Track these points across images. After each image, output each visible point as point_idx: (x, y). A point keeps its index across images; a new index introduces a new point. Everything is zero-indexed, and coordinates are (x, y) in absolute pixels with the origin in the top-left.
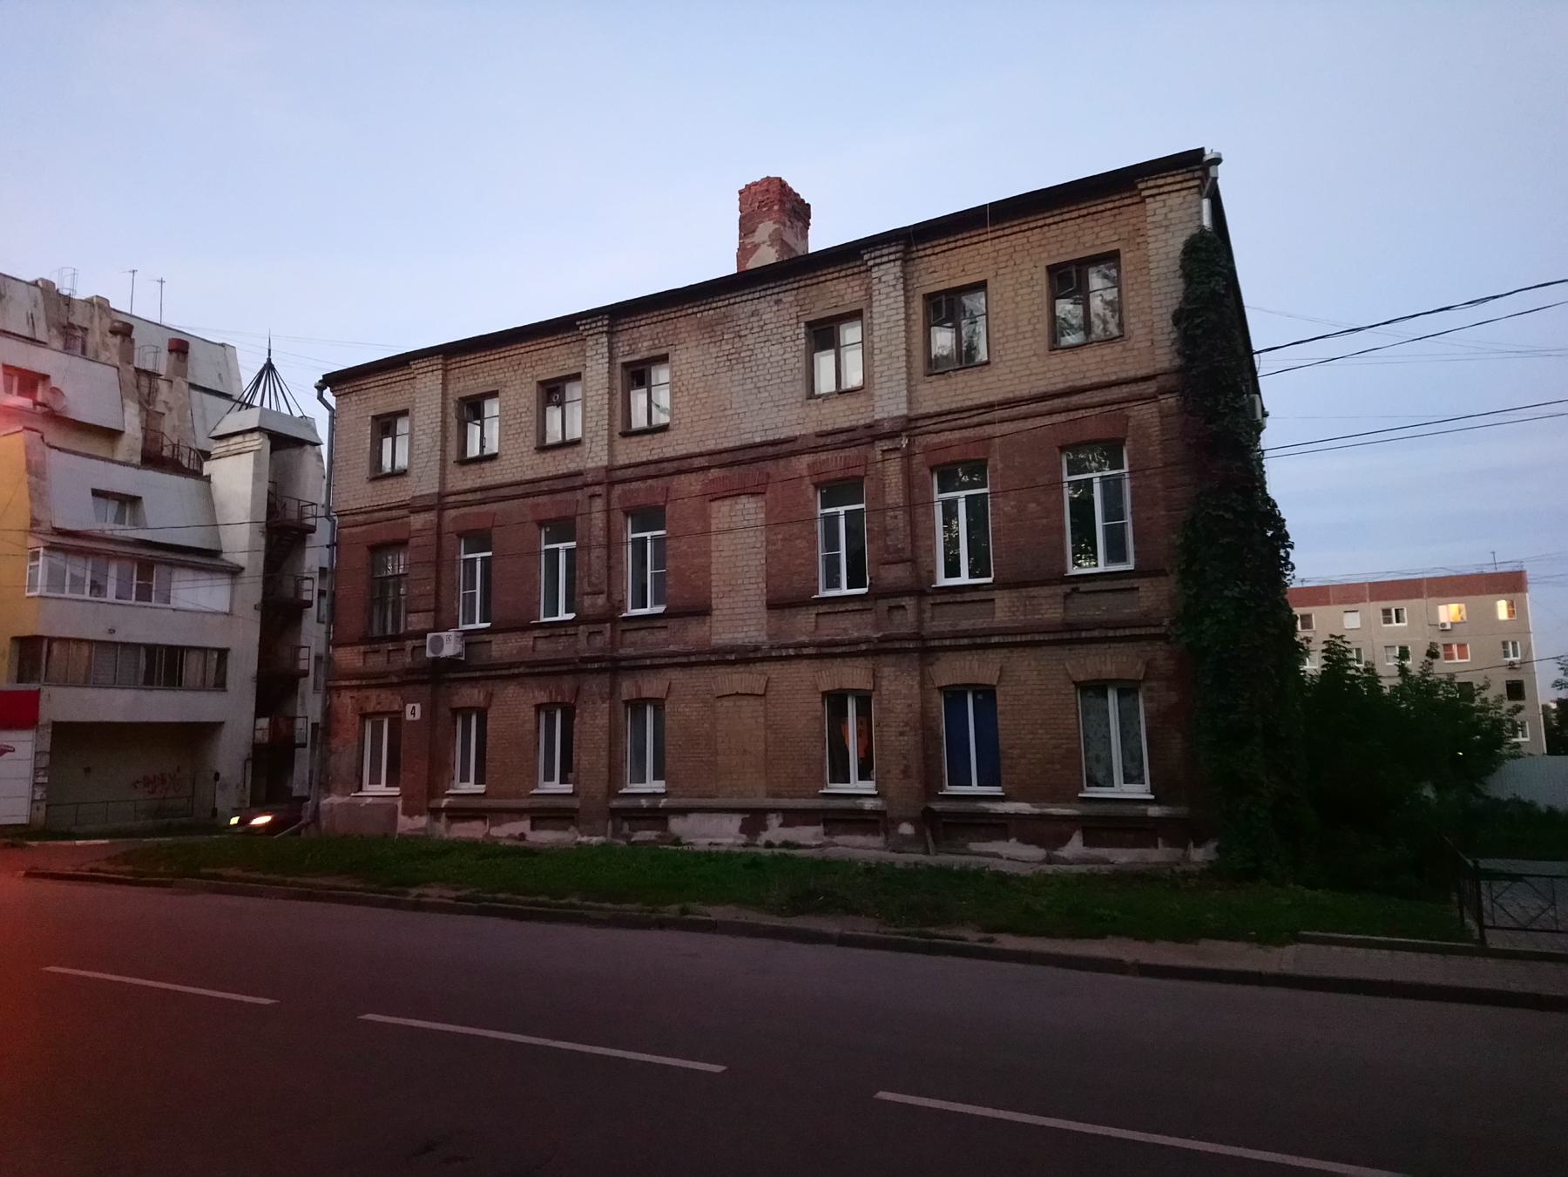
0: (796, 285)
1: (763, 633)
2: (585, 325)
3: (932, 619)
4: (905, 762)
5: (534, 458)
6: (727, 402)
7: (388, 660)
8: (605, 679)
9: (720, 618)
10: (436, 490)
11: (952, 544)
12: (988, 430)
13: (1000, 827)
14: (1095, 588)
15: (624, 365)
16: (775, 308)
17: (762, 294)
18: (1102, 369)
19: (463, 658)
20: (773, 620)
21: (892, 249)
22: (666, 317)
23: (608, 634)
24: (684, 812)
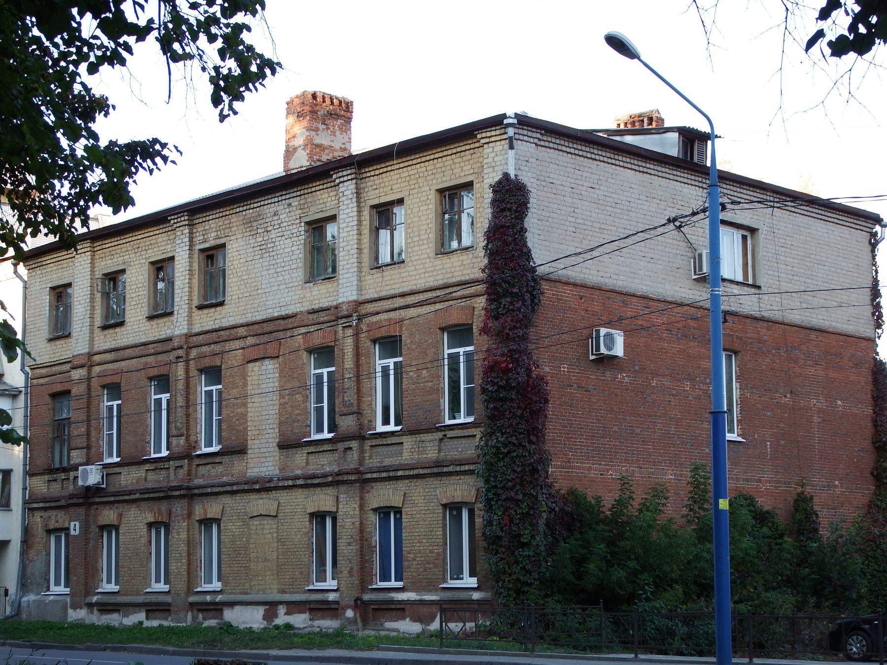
0: (298, 193)
1: (277, 468)
2: (174, 219)
3: (371, 458)
4: (350, 565)
5: (146, 324)
6: (259, 283)
7: (62, 487)
8: (184, 503)
9: (253, 456)
10: (87, 350)
11: (319, 411)
12: (403, 313)
13: (399, 610)
14: (466, 434)
15: (202, 251)
16: (287, 210)
17: (280, 198)
18: (462, 271)
19: (104, 486)
20: (282, 457)
21: (349, 172)
22: (224, 214)
23: (186, 468)
24: (232, 604)
